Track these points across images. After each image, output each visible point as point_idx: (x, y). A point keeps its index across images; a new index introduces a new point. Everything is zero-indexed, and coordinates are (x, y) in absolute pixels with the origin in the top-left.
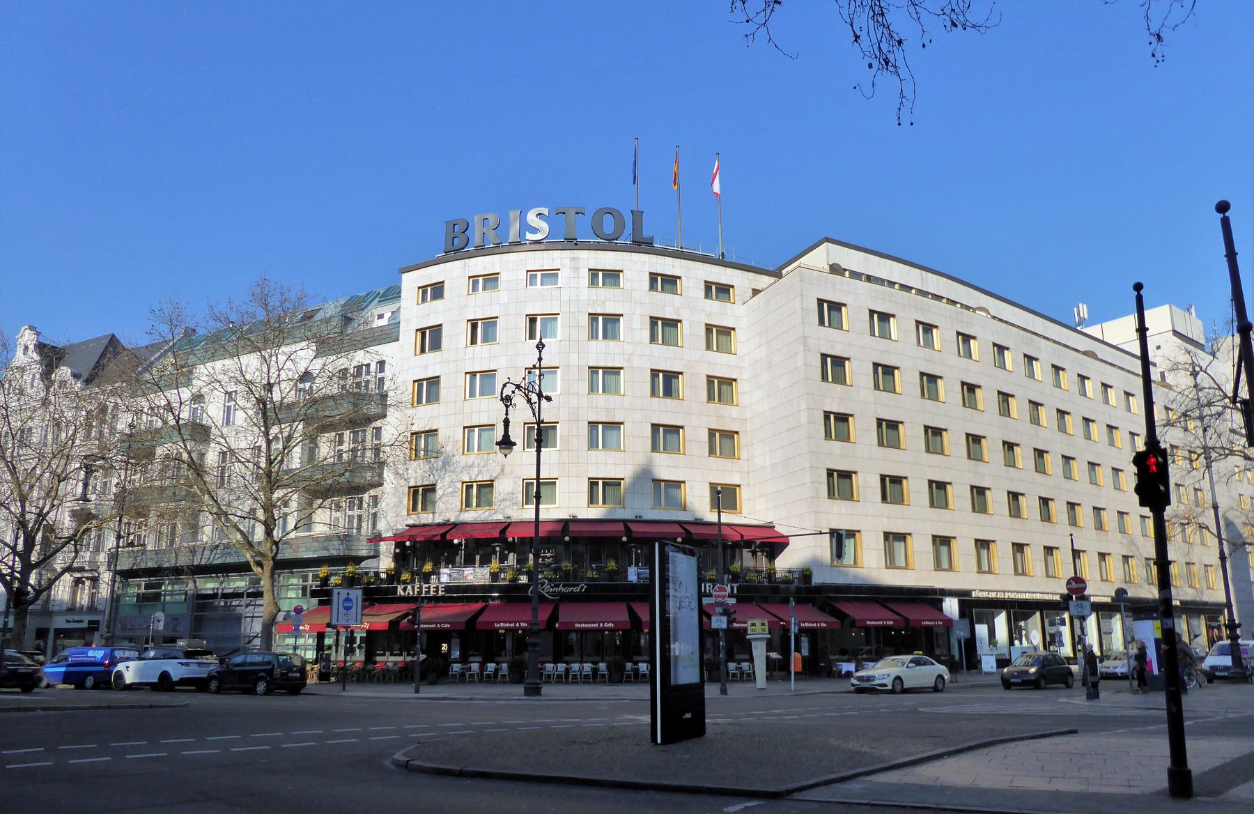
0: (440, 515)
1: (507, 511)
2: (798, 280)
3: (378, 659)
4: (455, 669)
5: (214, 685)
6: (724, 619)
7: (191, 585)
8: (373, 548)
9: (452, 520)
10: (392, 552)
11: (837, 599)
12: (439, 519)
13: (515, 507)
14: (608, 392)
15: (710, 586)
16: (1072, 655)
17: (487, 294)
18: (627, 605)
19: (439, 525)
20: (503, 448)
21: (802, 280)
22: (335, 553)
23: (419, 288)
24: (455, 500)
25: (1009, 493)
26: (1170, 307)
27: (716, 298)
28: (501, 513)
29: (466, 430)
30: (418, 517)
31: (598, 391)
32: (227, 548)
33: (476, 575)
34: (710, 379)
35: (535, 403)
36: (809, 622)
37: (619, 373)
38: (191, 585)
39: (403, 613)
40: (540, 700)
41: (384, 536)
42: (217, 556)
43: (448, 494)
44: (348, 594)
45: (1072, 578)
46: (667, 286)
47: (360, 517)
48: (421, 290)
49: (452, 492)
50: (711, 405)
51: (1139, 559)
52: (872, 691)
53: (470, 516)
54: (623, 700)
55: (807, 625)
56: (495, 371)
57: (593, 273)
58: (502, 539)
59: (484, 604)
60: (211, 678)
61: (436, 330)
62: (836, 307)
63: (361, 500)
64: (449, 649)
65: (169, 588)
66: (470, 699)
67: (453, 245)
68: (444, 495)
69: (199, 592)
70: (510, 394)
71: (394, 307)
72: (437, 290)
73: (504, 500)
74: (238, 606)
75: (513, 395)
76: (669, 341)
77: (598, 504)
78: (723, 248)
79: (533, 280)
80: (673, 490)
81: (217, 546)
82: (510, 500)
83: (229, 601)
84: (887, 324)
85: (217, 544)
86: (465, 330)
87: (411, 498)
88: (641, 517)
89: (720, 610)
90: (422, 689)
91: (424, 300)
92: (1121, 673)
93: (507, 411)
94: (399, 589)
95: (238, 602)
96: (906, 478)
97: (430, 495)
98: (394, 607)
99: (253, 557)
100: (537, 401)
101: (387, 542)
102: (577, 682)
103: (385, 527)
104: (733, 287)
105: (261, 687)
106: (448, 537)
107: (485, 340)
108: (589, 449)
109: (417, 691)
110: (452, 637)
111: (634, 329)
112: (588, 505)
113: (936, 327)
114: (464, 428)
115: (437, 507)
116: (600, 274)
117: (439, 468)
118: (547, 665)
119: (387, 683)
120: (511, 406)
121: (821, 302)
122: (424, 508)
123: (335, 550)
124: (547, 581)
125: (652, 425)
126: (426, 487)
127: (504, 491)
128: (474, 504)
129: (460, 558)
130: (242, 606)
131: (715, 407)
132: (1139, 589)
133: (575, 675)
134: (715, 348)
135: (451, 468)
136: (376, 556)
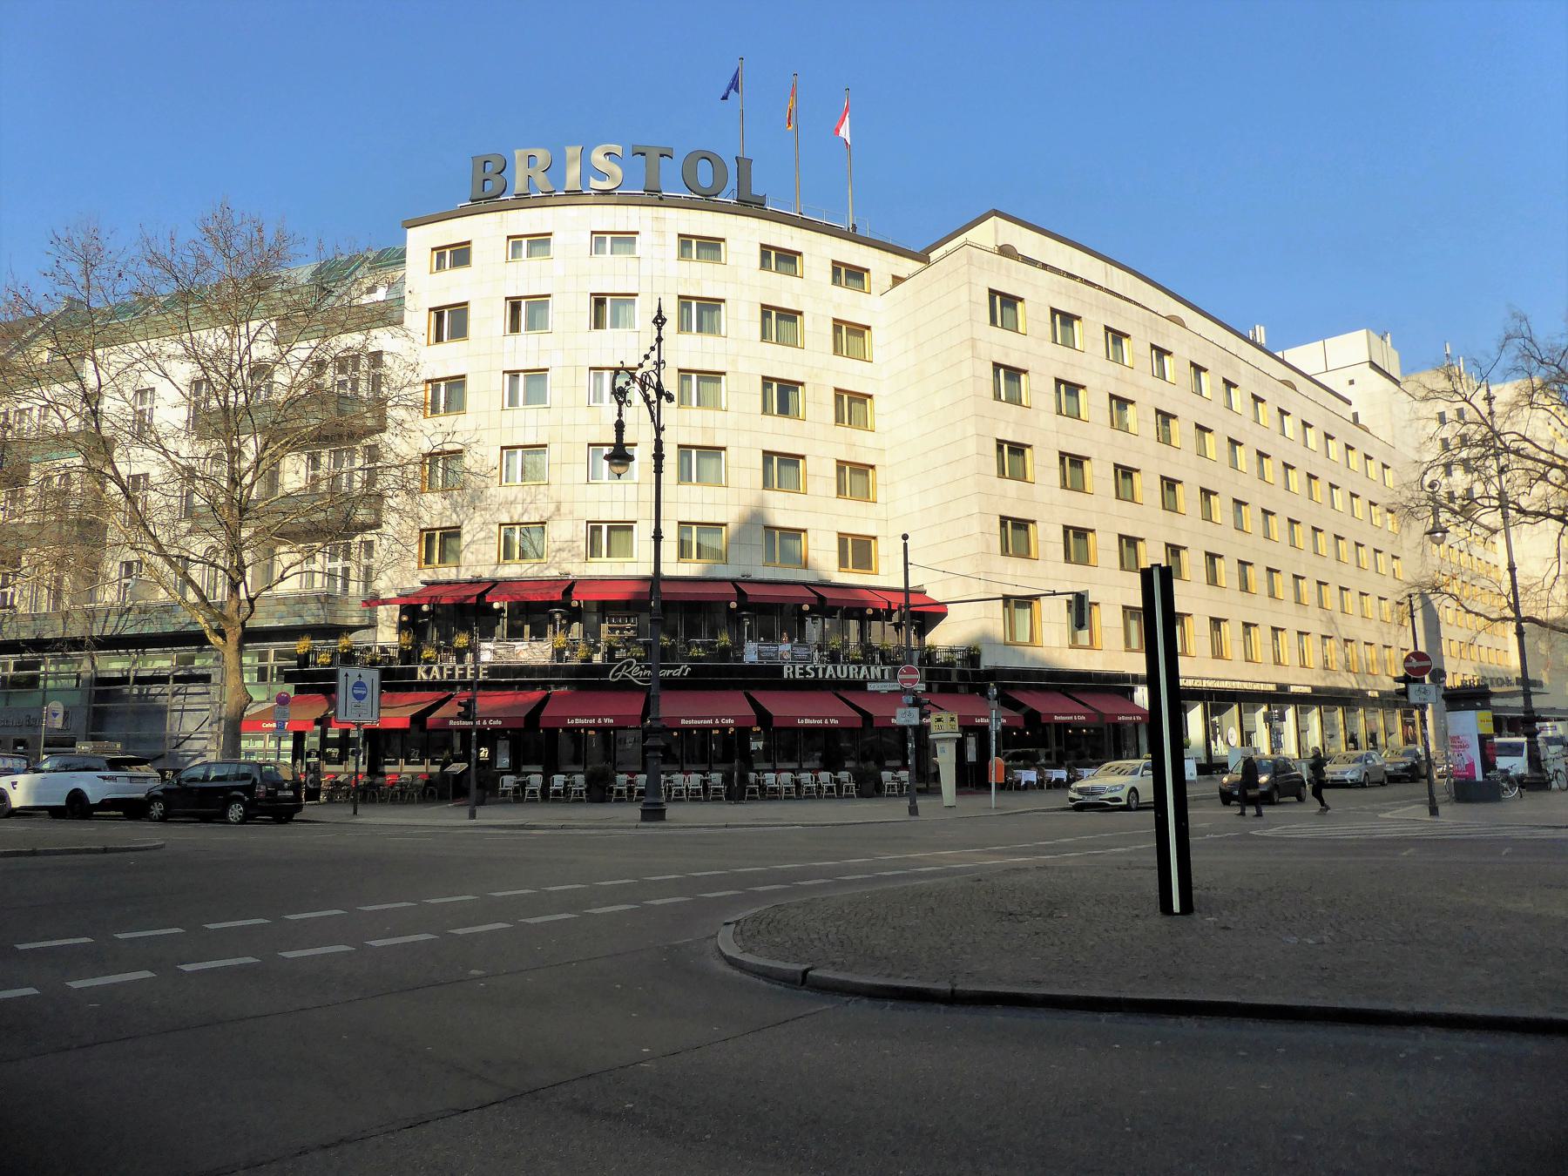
0: (467, 570)
1: (564, 565)
3: (388, 769)
5: (157, 809)
7: (86, 664)
8: (368, 614)
9: (486, 575)
10: (396, 619)
11: (1012, 687)
12: (465, 575)
13: (576, 560)
15: (854, 670)
16: (1297, 757)
17: (536, 262)
18: (745, 693)
19: (471, 583)
20: (616, 464)
21: (970, 263)
22: (311, 620)
23: (433, 249)
26: (1368, 333)
28: (556, 568)
29: (505, 451)
30: (435, 573)
31: (690, 404)
32: (145, 612)
33: (532, 652)
34: (839, 393)
35: (654, 402)
38: (86, 664)
39: (430, 704)
40: (664, 828)
41: (383, 597)
42: (128, 624)
43: (478, 540)
44: (360, 676)
45: (1412, 654)
47: (346, 570)
48: (435, 253)
49: (484, 538)
50: (840, 429)
51: (1338, 641)
52: (1101, 807)
53: (511, 571)
56: (547, 370)
59: (545, 692)
60: (151, 799)
62: (1011, 301)
65: (52, 669)
66: (562, 827)
68: (472, 542)
69: (99, 675)
71: (402, 272)
73: (560, 550)
74: (160, 694)
77: (690, 557)
79: (600, 246)
80: (787, 541)
81: (129, 609)
82: (569, 551)
83: (145, 687)
84: (1070, 329)
85: (128, 606)
86: (502, 312)
87: (424, 546)
88: (748, 576)
90: (480, 811)
92: (1351, 780)
93: (620, 410)
94: (419, 671)
97: (451, 543)
101: (387, 606)
103: (385, 585)
105: (235, 812)
106: (488, 599)
109: (473, 816)
110: (498, 738)
111: (741, 319)
113: (1127, 336)
114: (502, 448)
115: (462, 559)
117: (465, 504)
118: (639, 776)
119: (406, 804)
120: (624, 404)
121: (993, 293)
122: (442, 560)
124: (635, 661)
125: (764, 452)
126: (445, 531)
127: (560, 536)
128: (517, 555)
129: (502, 628)
130: (167, 694)
132: (1337, 677)
135: (483, 505)
136: (372, 626)
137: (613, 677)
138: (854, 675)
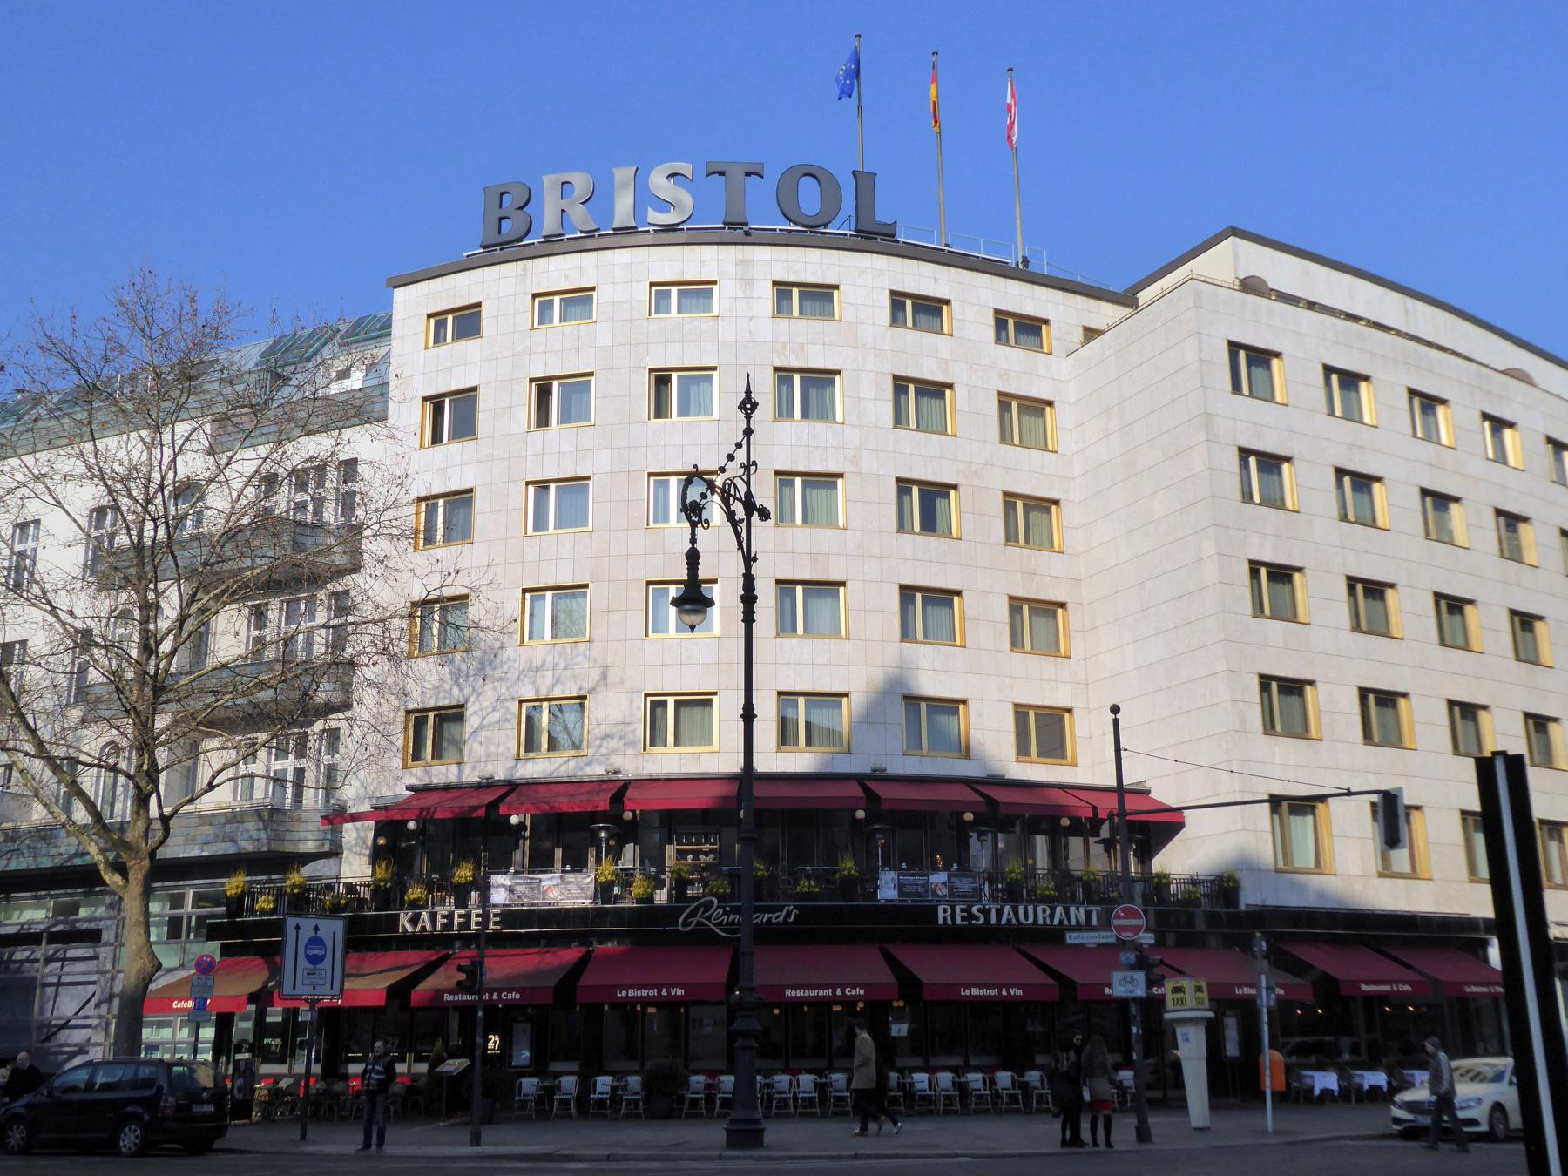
0: (474, 768)
2: (1192, 304)
4: (599, 1088)
6: (1140, 976)
8: (329, 836)
9: (500, 775)
10: (370, 843)
11: (1292, 938)
12: (471, 776)
13: (630, 751)
14: (813, 522)
15: (1044, 911)
17: (570, 327)
22: (247, 846)
24: (507, 736)
25: (1527, 715)
27: (1016, 343)
29: (528, 596)
30: (427, 773)
31: (793, 520)
32: (13, 840)
34: (1010, 499)
35: (741, 521)
36: (981, 986)
37: (834, 485)
40: (760, 1158)
43: (490, 724)
44: (316, 929)
46: (923, 319)
47: (300, 773)
48: (432, 321)
49: (499, 722)
50: (1013, 551)
53: (537, 768)
54: (957, 1156)
55: (974, 991)
57: (782, 289)
58: (612, 817)
59: (584, 949)
61: (466, 398)
62: (1261, 358)
63: (304, 738)
64: (506, 1045)
66: (609, 1158)
67: (500, 232)
68: (481, 727)
70: (698, 499)
72: (467, 321)
74: (27, 960)
75: (704, 501)
76: (933, 425)
78: (1024, 250)
79: (663, 302)
86: (525, 398)
89: (1129, 957)
90: (487, 1133)
91: (439, 339)
95: (28, 953)
96: (1404, 695)
97: (450, 729)
98: (391, 958)
99: (102, 851)
100: (744, 517)
101: (359, 824)
102: (788, 1115)
103: (353, 794)
104: (1046, 322)
105: (130, 1138)
106: (502, 810)
107: (565, 418)
108: (778, 635)
112: (778, 747)
114: (525, 591)
115: (466, 751)
116: (795, 291)
120: (700, 525)
122: (438, 754)
123: (250, 839)
124: (716, 901)
126: (442, 712)
128: (545, 745)
131: (1018, 554)
133: (785, 1101)
134: (1016, 441)
135: (497, 673)
136: (335, 853)
137: (685, 924)
138: (945, 919)
